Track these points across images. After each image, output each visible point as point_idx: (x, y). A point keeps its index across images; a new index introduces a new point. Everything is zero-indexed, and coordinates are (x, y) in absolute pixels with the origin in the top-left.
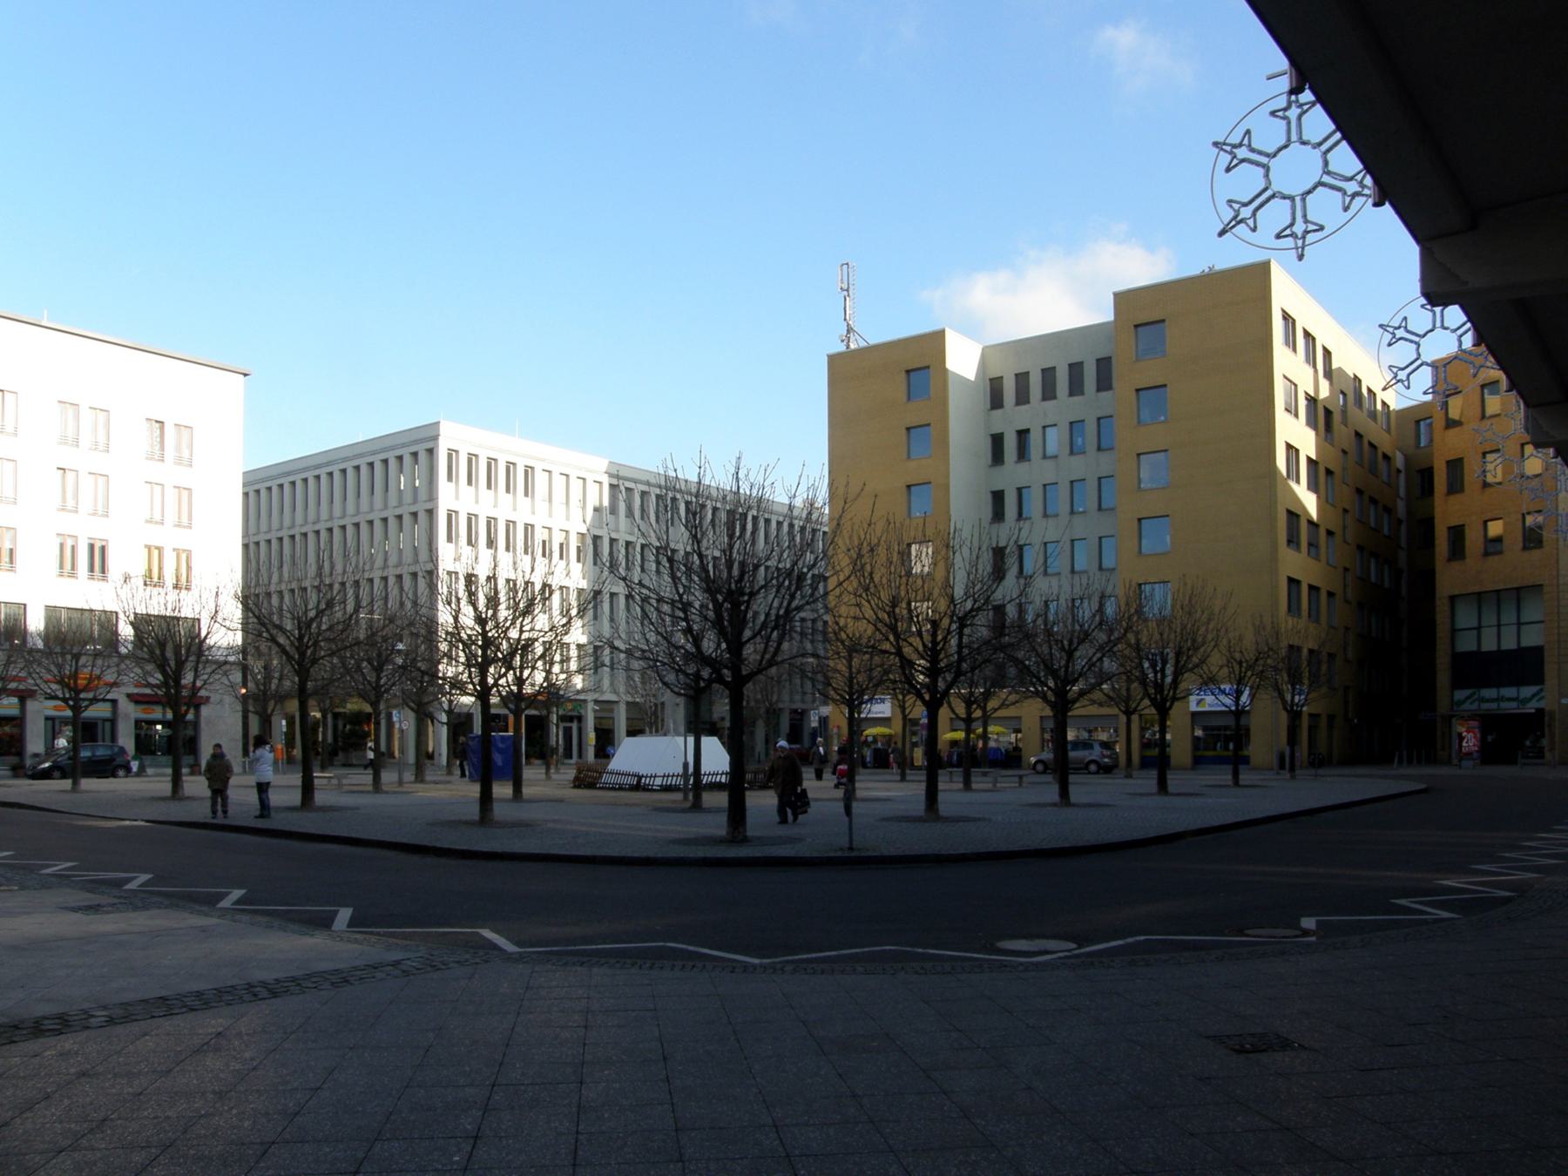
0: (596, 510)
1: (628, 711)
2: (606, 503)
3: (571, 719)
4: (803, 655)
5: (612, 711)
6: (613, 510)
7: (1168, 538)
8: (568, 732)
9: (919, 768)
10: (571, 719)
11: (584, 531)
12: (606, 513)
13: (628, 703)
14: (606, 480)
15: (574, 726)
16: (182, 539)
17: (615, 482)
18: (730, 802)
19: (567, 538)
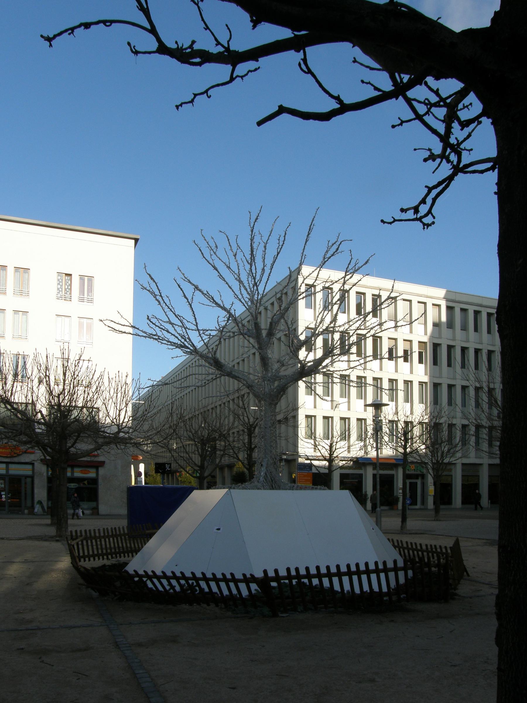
0: (435, 325)
1: (463, 470)
2: (444, 319)
3: (416, 477)
4: (184, 469)
5: (450, 470)
6: (450, 324)
7: (49, 450)
8: (413, 487)
9: (430, 510)
10: (416, 477)
11: (425, 339)
12: (444, 328)
13: (490, 465)
14: (444, 304)
15: (419, 482)
16: (64, 307)
17: (451, 304)
18: (502, 526)
19: (396, 345)
